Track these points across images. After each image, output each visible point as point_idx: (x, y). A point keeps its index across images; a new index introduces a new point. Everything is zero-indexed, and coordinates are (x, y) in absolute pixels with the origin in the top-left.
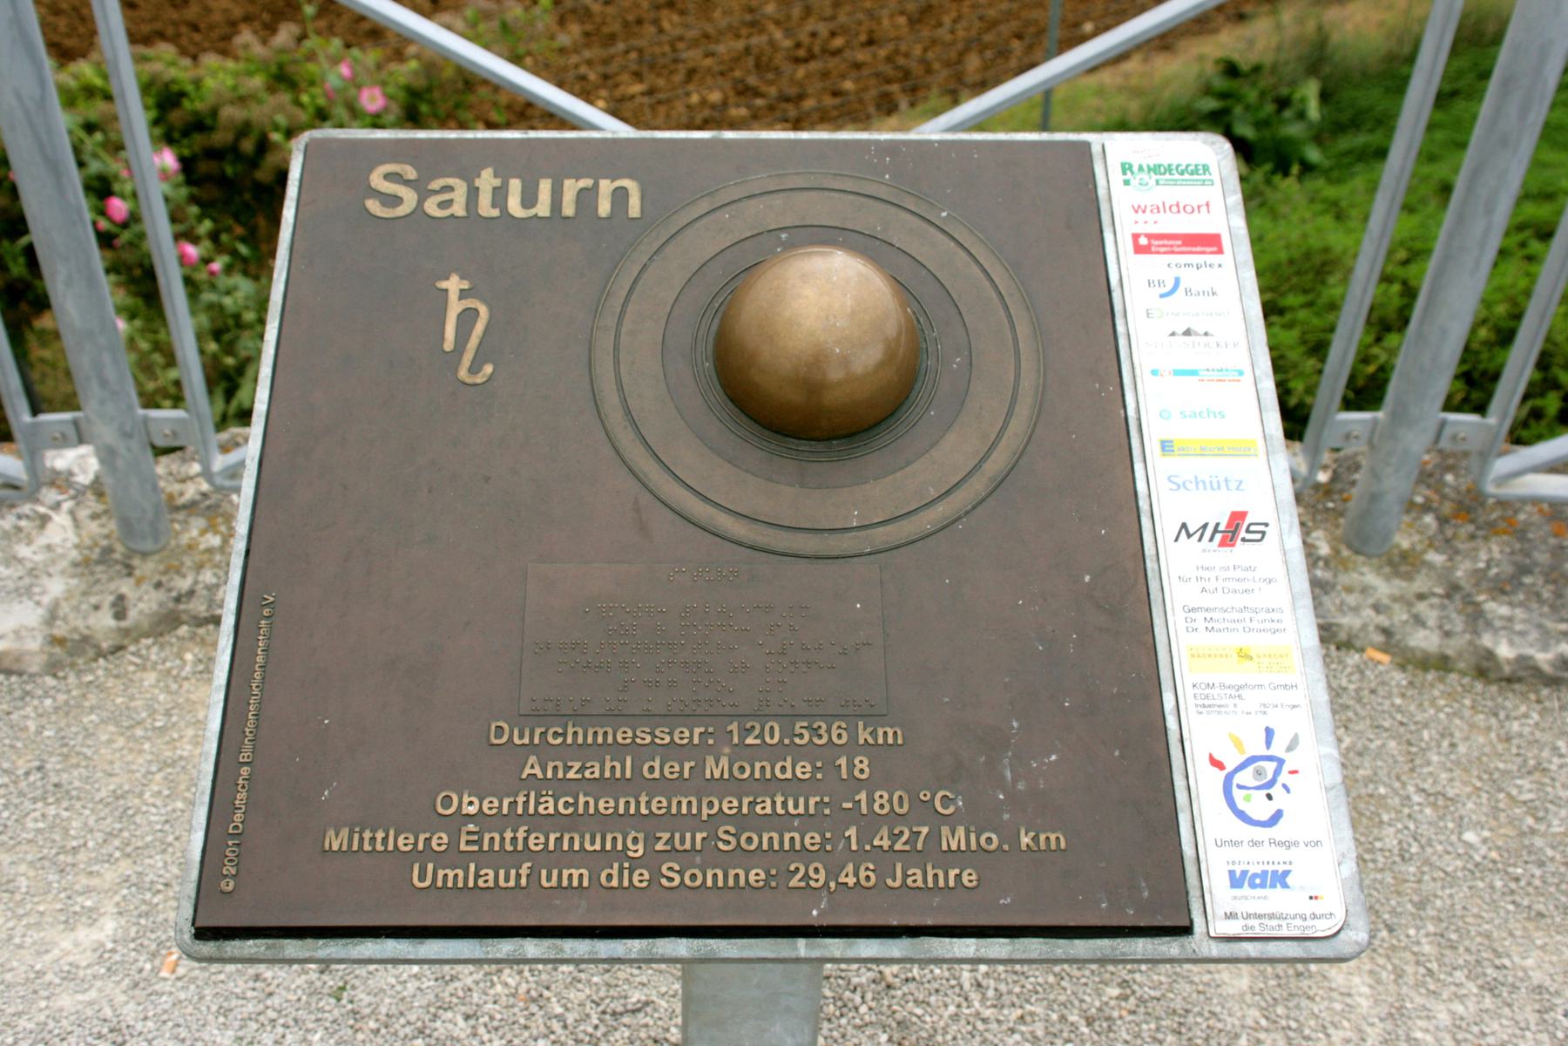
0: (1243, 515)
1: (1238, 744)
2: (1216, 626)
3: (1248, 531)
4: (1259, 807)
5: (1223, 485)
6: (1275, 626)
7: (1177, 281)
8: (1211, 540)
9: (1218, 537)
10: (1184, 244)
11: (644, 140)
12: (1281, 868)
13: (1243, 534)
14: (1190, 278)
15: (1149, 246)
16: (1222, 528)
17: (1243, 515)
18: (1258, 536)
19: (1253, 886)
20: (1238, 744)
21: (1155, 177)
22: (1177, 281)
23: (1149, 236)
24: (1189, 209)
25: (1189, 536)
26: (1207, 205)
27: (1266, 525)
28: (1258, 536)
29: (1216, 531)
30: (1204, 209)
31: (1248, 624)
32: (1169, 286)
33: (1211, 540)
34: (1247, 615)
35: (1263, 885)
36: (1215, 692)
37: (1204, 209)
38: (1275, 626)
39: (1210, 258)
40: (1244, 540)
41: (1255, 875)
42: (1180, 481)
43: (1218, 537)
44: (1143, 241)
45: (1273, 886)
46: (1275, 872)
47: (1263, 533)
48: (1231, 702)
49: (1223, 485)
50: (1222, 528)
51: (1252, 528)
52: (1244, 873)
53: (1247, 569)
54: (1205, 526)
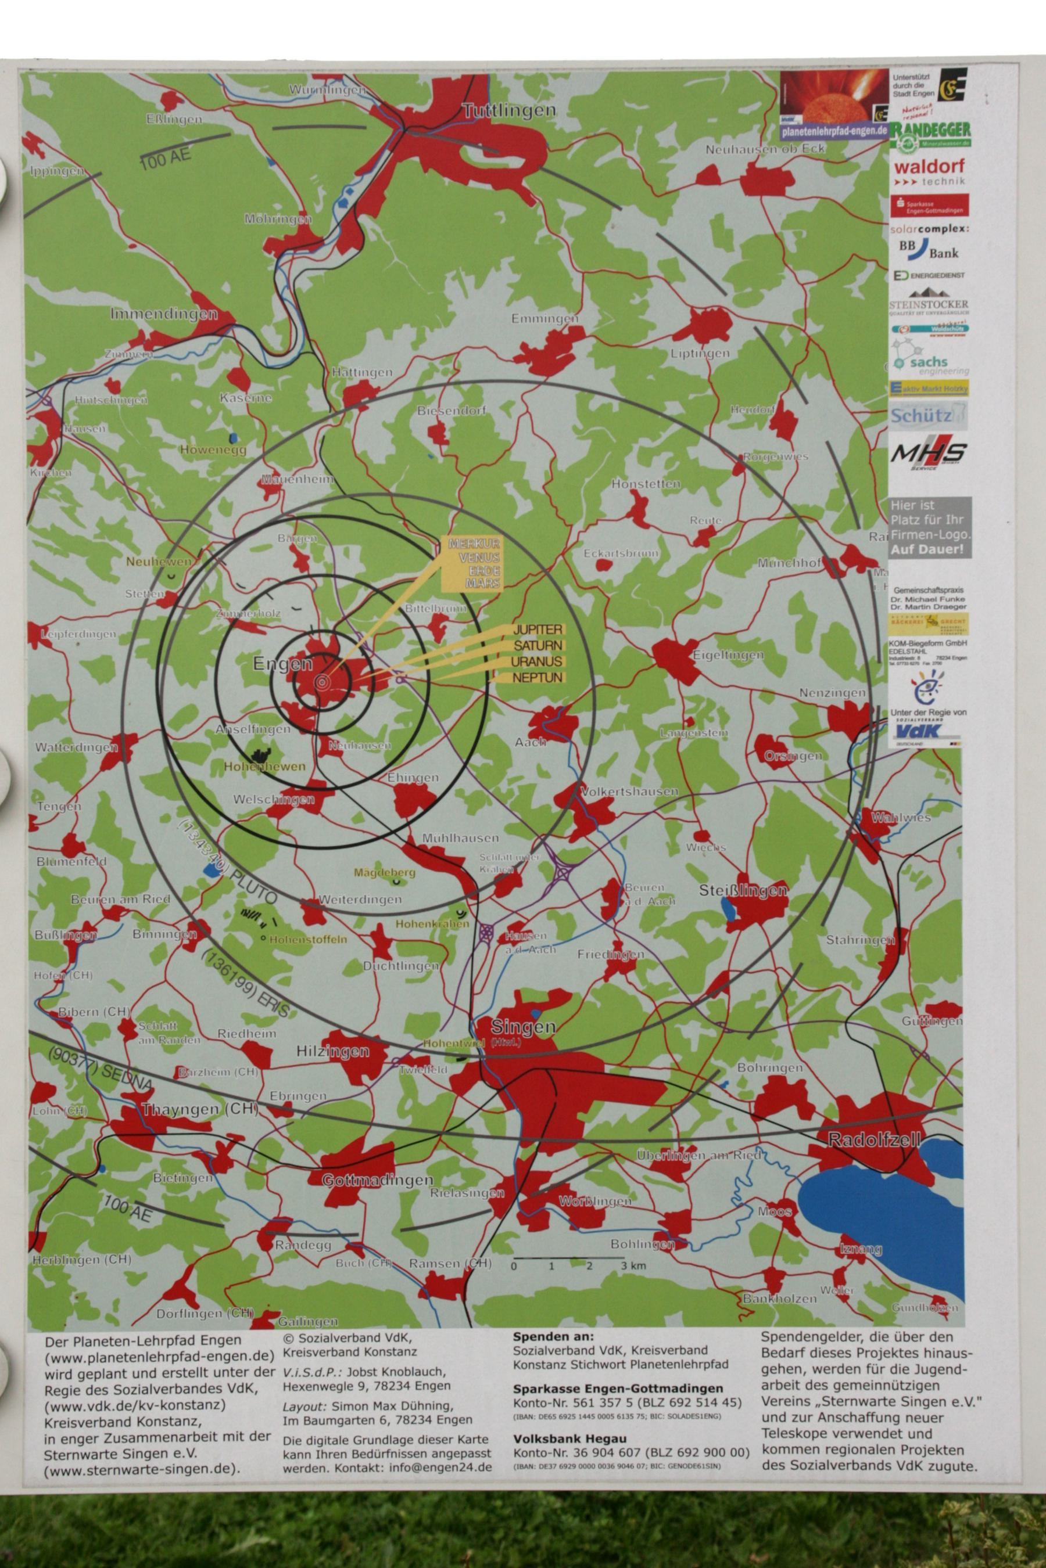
0: (948, 437)
1: (922, 675)
2: (914, 604)
3: (950, 452)
4: (926, 698)
5: (935, 417)
6: (959, 603)
7: (926, 242)
8: (920, 459)
9: (927, 456)
10: (935, 207)
11: (479, 189)
12: (934, 724)
13: (945, 454)
14: (937, 241)
15: (906, 207)
16: (930, 449)
17: (948, 437)
18: (957, 456)
19: (913, 736)
20: (922, 675)
21: (919, 138)
22: (926, 242)
23: (907, 198)
24: (945, 168)
25: (903, 456)
26: (962, 162)
27: (965, 446)
28: (957, 456)
29: (925, 452)
30: (958, 167)
31: (938, 602)
32: (918, 246)
33: (920, 459)
34: (938, 595)
35: (920, 736)
36: (906, 648)
37: (958, 167)
38: (959, 603)
39: (957, 221)
40: (946, 459)
41: (916, 728)
42: (901, 414)
43: (927, 456)
44: (901, 203)
45: (927, 736)
46: (929, 726)
47: (961, 453)
48: (916, 655)
49: (935, 417)
50: (930, 449)
51: (954, 449)
52: (908, 727)
53: (952, 1451)
54: (918, 447)
